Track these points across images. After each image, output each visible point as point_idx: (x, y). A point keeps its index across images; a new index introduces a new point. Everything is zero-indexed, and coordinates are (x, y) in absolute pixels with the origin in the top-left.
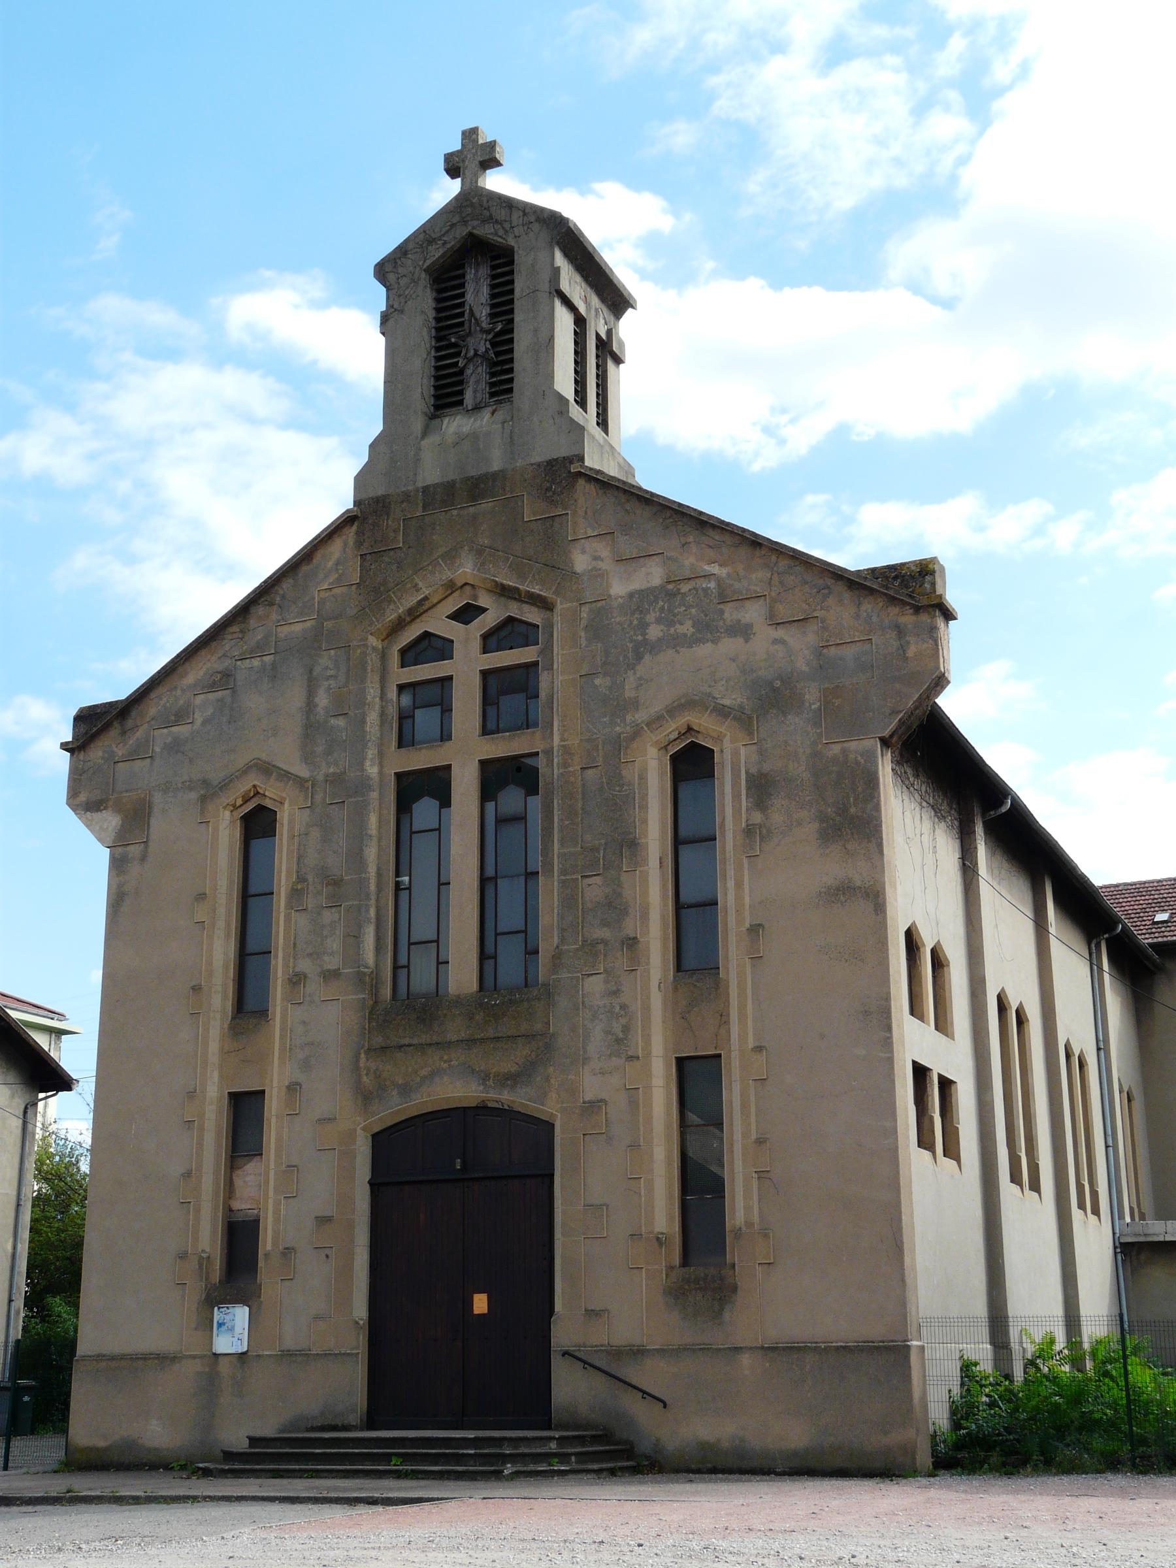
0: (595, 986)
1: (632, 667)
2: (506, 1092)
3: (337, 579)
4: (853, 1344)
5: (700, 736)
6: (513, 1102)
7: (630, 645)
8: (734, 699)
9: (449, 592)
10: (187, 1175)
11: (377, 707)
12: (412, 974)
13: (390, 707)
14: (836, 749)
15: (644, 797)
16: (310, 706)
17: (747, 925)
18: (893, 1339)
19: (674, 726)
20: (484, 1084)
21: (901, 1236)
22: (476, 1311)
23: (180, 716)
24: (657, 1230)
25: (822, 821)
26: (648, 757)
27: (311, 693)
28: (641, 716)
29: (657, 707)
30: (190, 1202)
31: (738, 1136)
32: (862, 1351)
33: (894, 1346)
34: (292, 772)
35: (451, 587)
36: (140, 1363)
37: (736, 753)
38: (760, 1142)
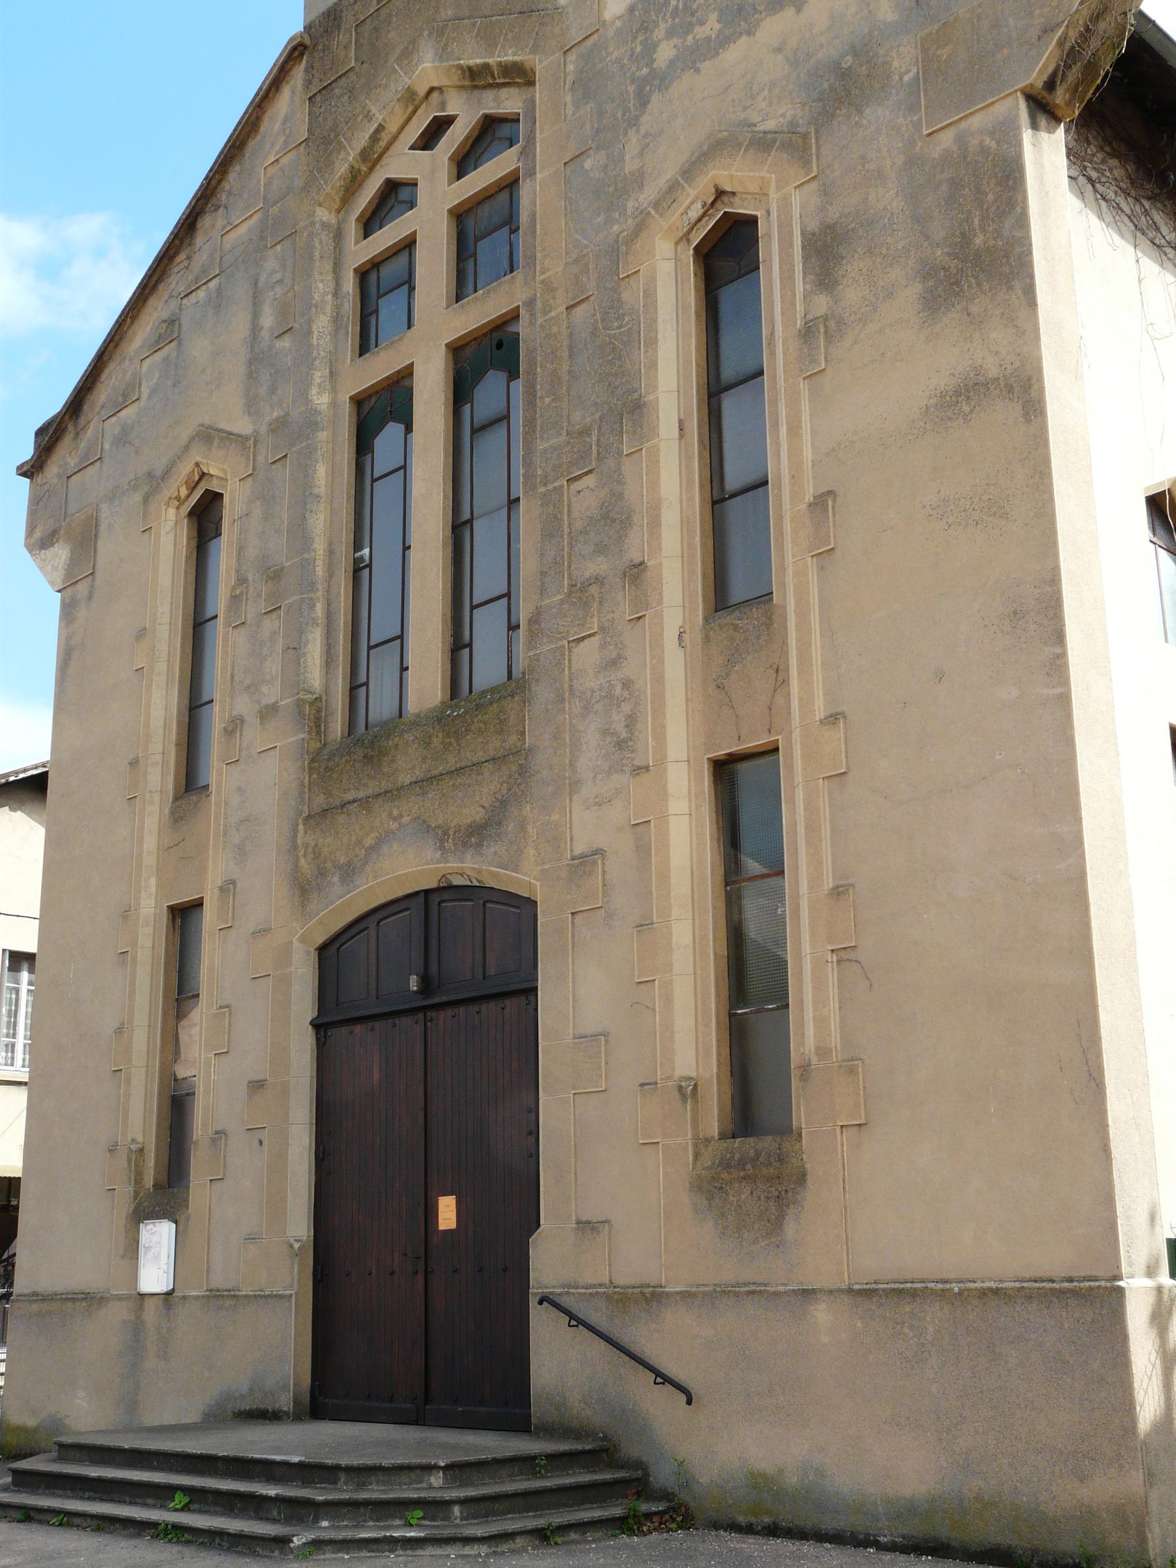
0: (587, 655)
1: (633, 122)
2: (469, 855)
3: (285, 141)
4: (1013, 1284)
5: (737, 200)
6: (479, 871)
7: (631, 89)
8: (783, 115)
9: (411, 108)
10: (120, 1030)
11: (328, 309)
12: (371, 693)
13: (347, 304)
14: (947, 139)
15: (652, 327)
16: (255, 329)
17: (809, 498)
18: (1093, 1273)
19: (692, 192)
20: (442, 848)
21: (1099, 1055)
22: (442, 1227)
23: (126, 398)
24: (679, 1072)
25: (926, 277)
26: (657, 258)
27: (256, 315)
28: (648, 195)
29: (670, 172)
30: (121, 1070)
31: (804, 888)
32: (1029, 1298)
33: (1091, 1289)
34: (235, 431)
35: (412, 101)
36: (70, 1305)
37: (785, 203)
38: (839, 894)
